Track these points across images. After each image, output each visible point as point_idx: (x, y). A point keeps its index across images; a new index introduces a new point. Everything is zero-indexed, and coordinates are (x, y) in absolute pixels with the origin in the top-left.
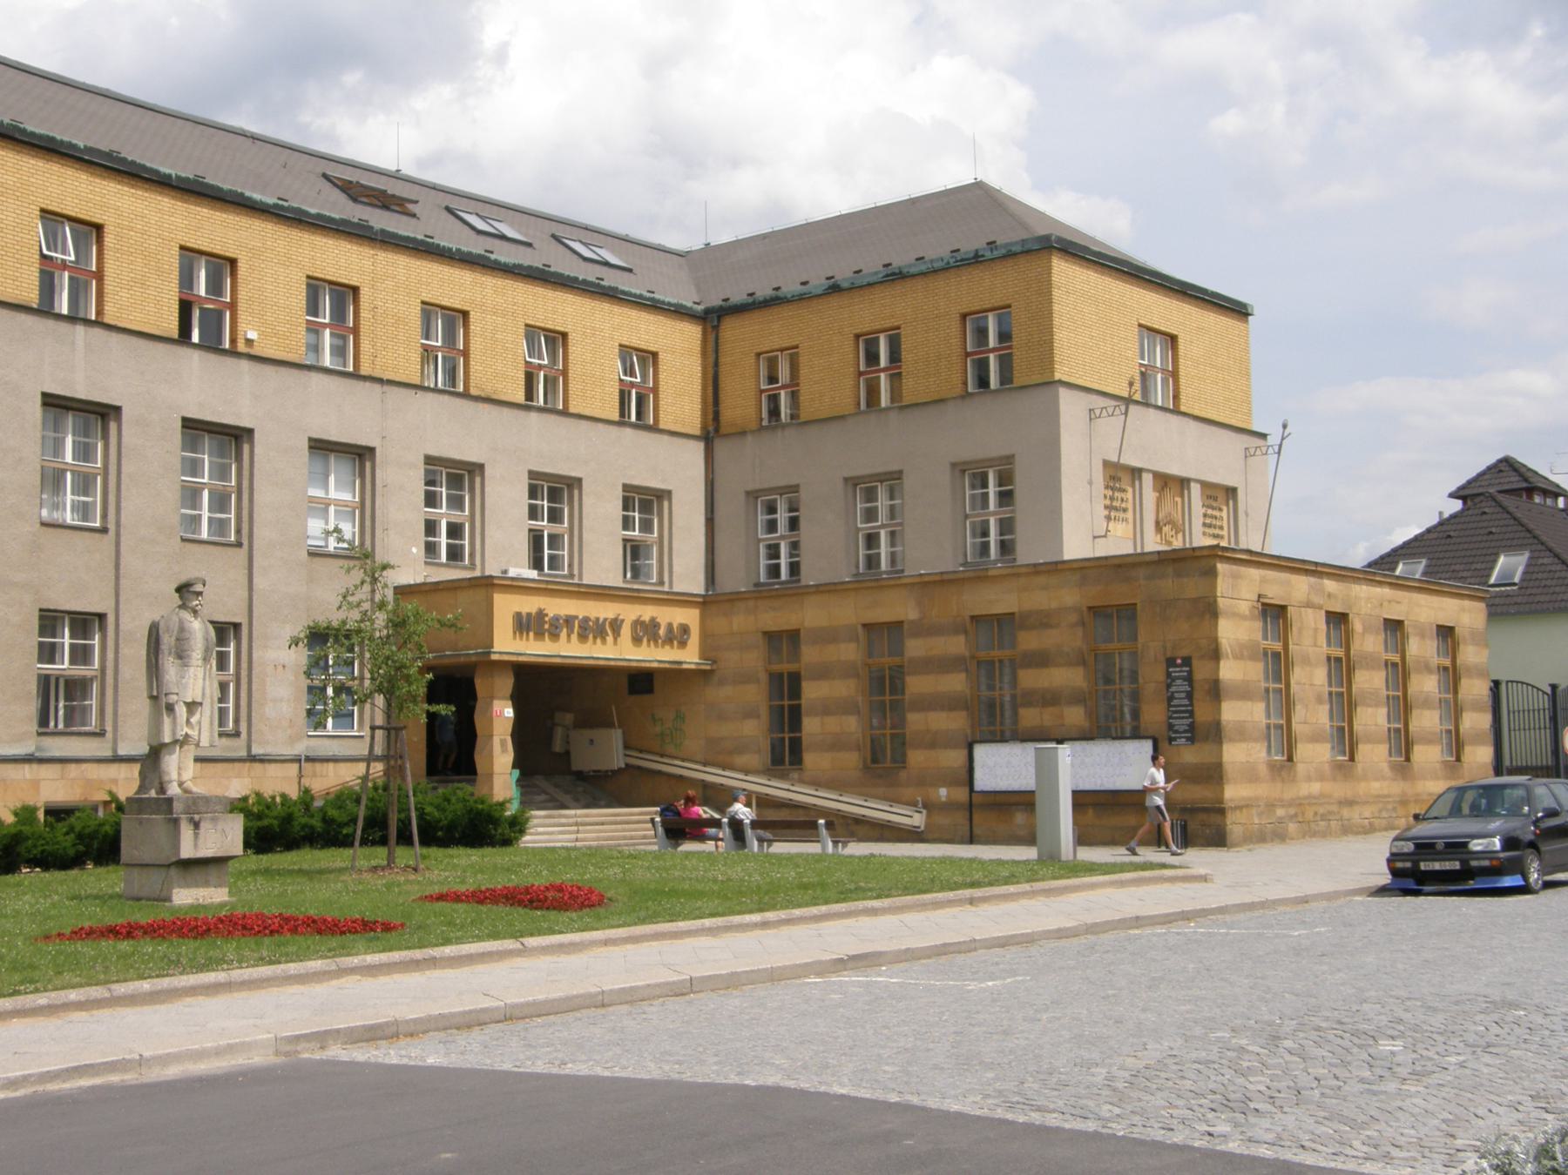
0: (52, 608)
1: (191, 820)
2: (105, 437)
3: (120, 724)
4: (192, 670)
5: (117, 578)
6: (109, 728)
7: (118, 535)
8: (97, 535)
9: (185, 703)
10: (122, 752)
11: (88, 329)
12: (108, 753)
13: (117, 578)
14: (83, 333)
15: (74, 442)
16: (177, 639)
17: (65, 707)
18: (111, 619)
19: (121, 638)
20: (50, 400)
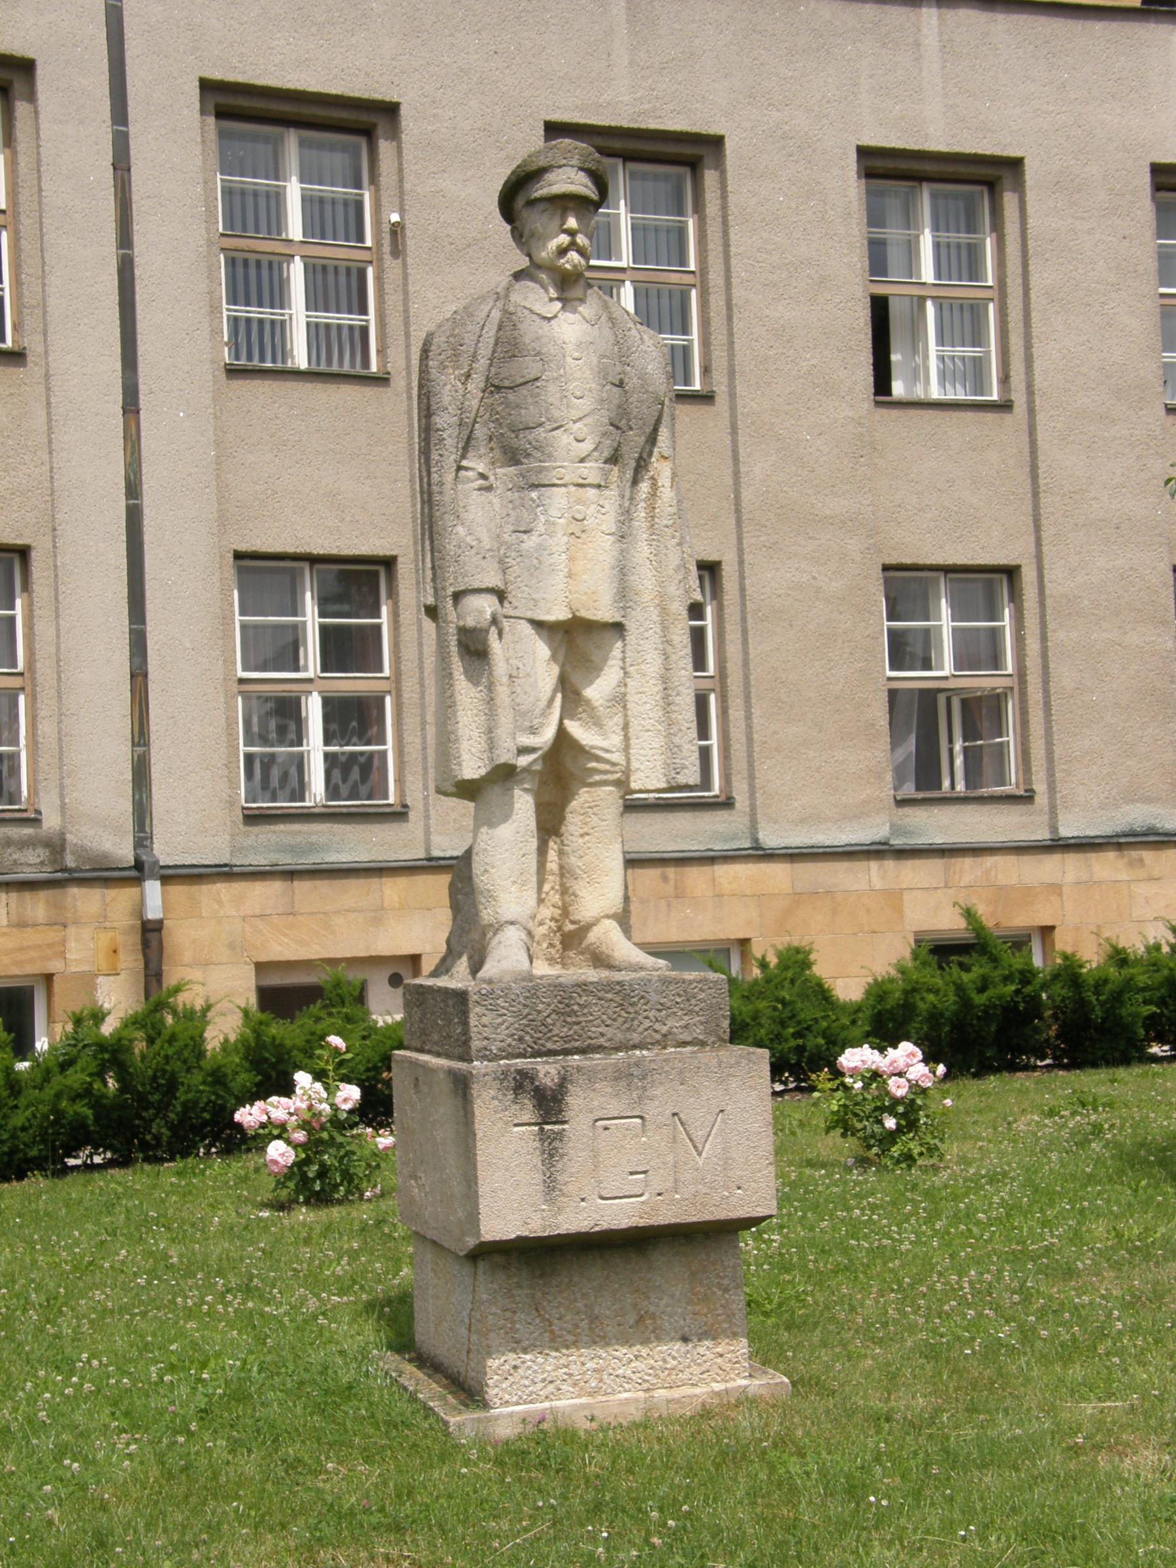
0: (908, 561)
1: (522, 1083)
2: (997, 226)
3: (1059, 775)
4: (558, 500)
5: (1035, 494)
6: (1040, 787)
7: (1031, 411)
8: (990, 417)
9: (538, 625)
10: (1067, 831)
11: (944, 11)
12: (1042, 834)
13: (1035, 494)
14: (934, 22)
15: (937, 246)
16: (493, 387)
17: (966, 750)
18: (1028, 576)
19: (1049, 611)
20: (879, 164)
